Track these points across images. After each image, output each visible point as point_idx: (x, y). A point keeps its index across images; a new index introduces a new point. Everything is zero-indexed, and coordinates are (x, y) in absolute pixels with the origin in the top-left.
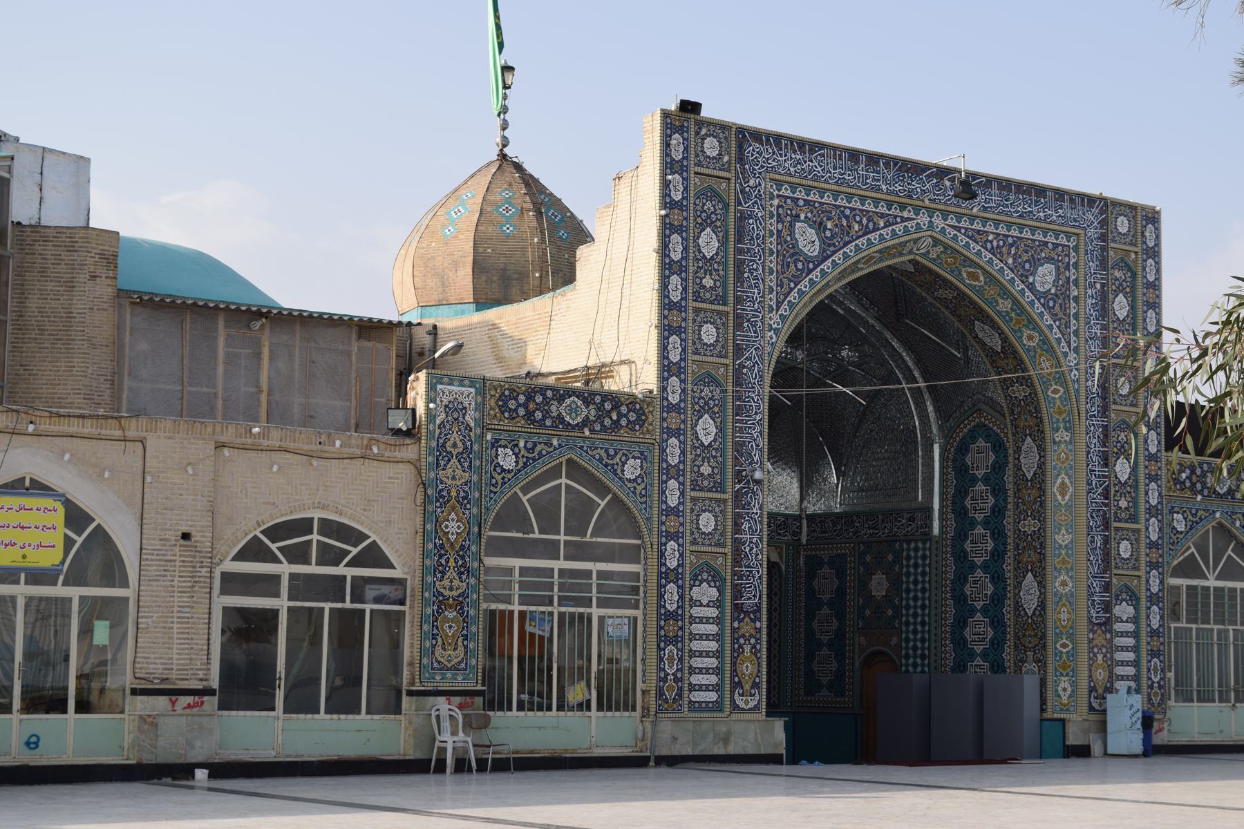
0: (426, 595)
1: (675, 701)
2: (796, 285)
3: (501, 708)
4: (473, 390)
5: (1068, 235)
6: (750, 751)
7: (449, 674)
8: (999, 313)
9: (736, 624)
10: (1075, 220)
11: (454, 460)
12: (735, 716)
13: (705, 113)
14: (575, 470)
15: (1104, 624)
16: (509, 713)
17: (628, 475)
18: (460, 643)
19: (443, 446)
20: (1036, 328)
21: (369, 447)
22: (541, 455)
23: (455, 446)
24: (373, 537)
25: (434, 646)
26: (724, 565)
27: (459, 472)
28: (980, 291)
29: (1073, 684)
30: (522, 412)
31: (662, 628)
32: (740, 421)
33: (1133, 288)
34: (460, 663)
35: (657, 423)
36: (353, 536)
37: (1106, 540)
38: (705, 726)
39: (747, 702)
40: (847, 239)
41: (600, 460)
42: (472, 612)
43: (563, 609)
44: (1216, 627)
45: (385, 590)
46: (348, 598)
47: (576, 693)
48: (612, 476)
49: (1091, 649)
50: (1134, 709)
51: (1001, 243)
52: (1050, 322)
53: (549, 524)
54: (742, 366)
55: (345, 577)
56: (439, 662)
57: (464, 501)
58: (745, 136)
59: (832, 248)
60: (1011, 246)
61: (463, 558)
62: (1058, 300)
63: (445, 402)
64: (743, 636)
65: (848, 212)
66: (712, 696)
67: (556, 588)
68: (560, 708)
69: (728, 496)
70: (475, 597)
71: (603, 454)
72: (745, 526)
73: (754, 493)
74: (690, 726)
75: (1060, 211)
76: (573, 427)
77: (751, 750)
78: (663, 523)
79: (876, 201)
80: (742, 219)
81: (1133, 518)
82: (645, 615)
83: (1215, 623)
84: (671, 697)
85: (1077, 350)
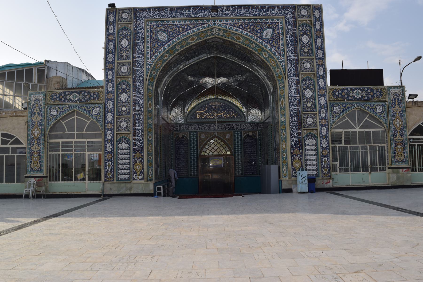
0: (392, 142)
1: (111, 178)
2: (158, 50)
3: (56, 181)
4: (42, 95)
5: (278, 19)
6: (140, 192)
7: (35, 172)
8: (252, 49)
9: (134, 154)
10: (280, 13)
11: (37, 114)
12: (133, 182)
13: (117, 6)
14: (79, 114)
15: (299, 147)
16: (59, 182)
17: (94, 113)
18: (38, 163)
19: (33, 111)
20: (265, 51)
21: (13, 113)
22: (65, 110)
23: (37, 110)
24: (16, 137)
25: (395, 156)
26: (130, 136)
27: (38, 117)
28: (243, 43)
29: (287, 168)
30: (375, 92)
31: (106, 156)
32: (134, 93)
33: (311, 33)
34: (403, 160)
35: (104, 97)
36: (11, 137)
37: (299, 118)
38: (122, 185)
39: (138, 178)
40: (178, 34)
41: (85, 110)
42: (42, 155)
43: (76, 153)
44: (360, 145)
45: (22, 150)
46: (10, 153)
47: (80, 176)
48: (89, 114)
49: (292, 156)
50: (304, 176)
51: (246, 25)
52: (270, 48)
53: (71, 129)
54: (135, 77)
55: (9, 147)
56: (32, 169)
57: (39, 125)
58: (136, 10)
59: (172, 37)
60: (251, 26)
61: (39, 140)
62: (274, 40)
63: (34, 99)
64: (295, 155)
65: (179, 25)
66: (127, 176)
67: (73, 147)
68: (75, 180)
69: (130, 116)
70: (43, 150)
71: (86, 108)
72: (137, 124)
73: (140, 114)
74: (117, 185)
75: (273, 12)
76: (75, 101)
77: (140, 192)
78: (106, 126)
79: (191, 21)
80: (135, 34)
81: (315, 110)
82: (387, 145)
83: (359, 144)
84: (114, 176)
85: (283, 56)
